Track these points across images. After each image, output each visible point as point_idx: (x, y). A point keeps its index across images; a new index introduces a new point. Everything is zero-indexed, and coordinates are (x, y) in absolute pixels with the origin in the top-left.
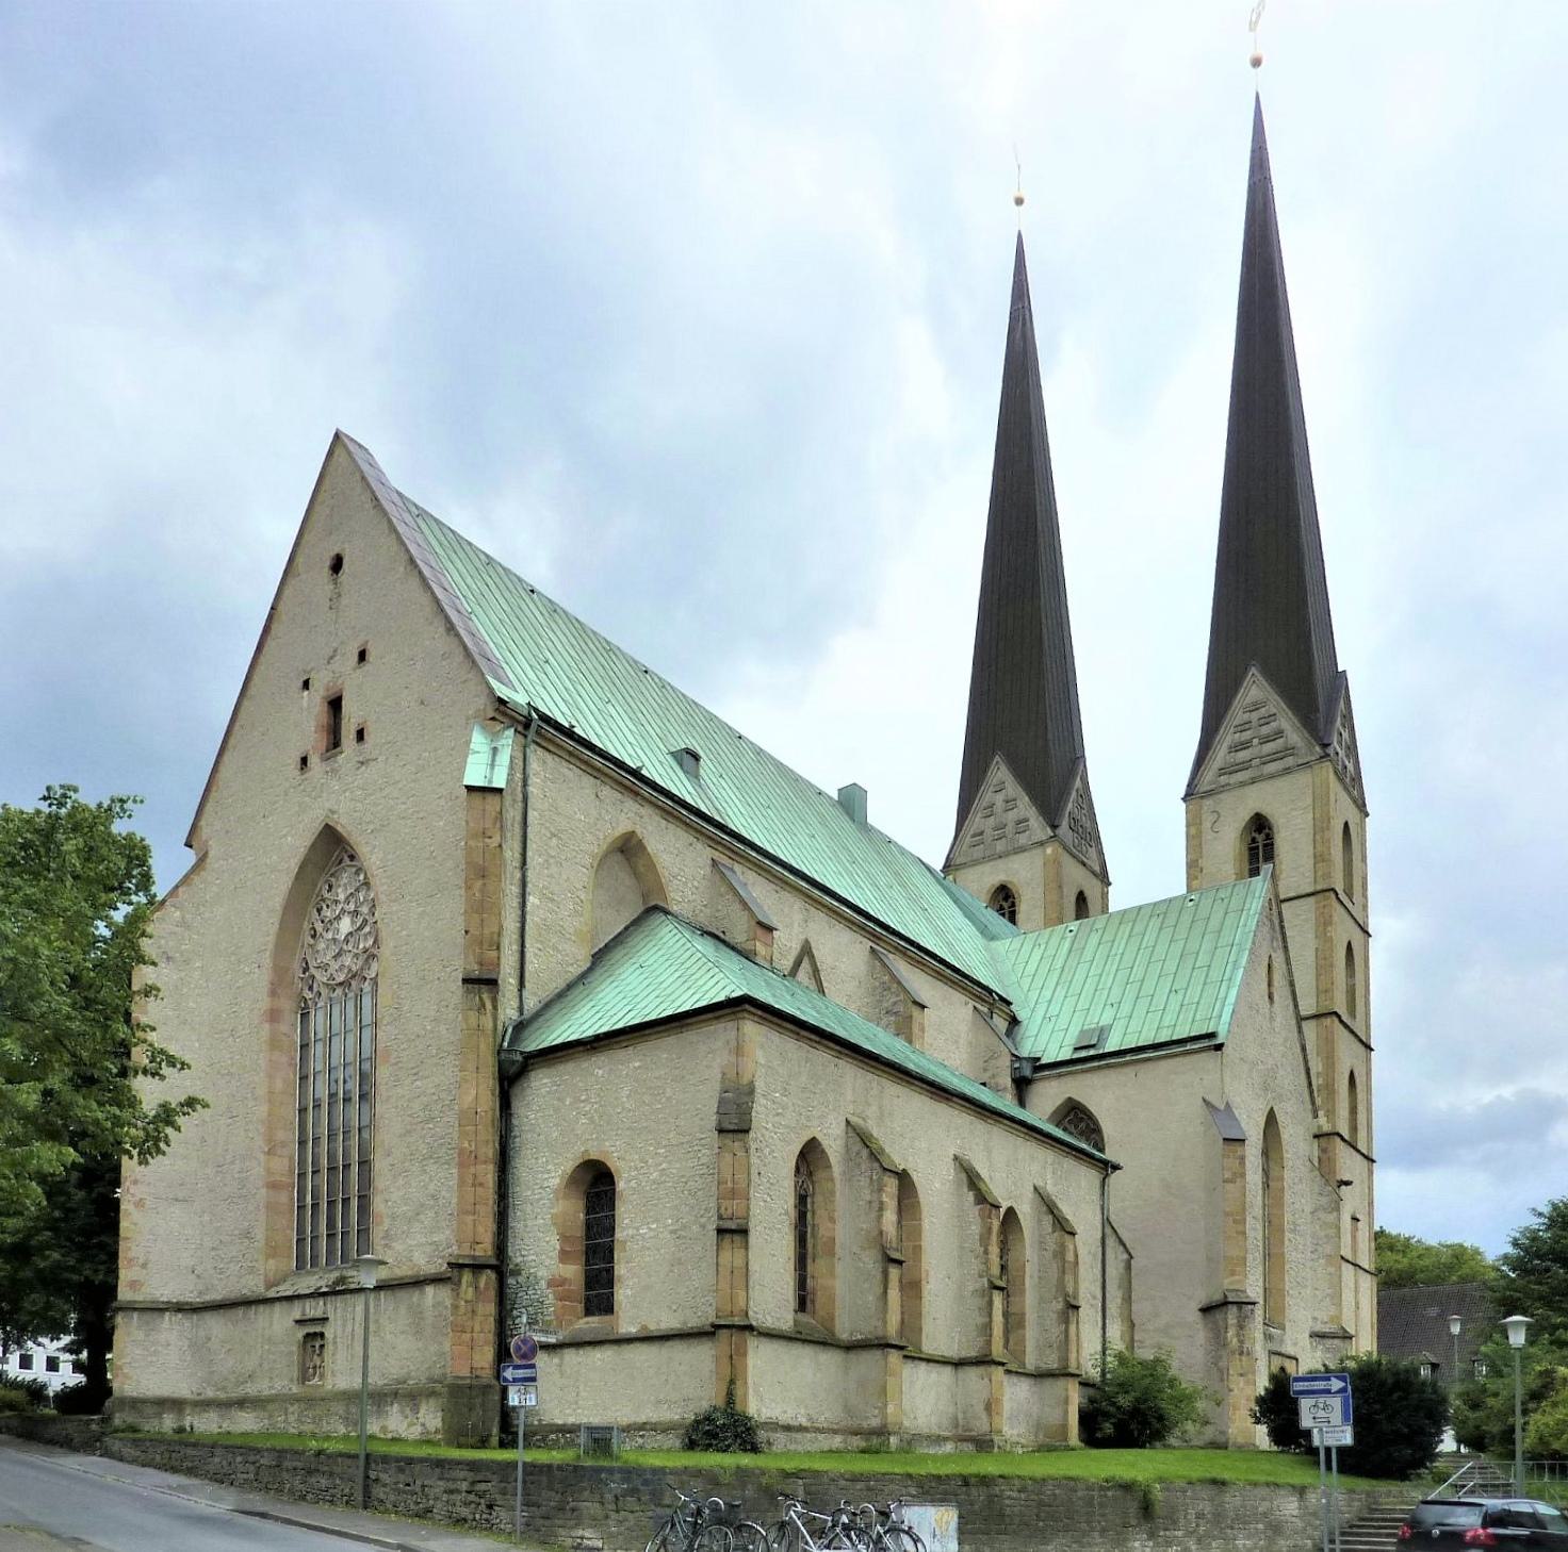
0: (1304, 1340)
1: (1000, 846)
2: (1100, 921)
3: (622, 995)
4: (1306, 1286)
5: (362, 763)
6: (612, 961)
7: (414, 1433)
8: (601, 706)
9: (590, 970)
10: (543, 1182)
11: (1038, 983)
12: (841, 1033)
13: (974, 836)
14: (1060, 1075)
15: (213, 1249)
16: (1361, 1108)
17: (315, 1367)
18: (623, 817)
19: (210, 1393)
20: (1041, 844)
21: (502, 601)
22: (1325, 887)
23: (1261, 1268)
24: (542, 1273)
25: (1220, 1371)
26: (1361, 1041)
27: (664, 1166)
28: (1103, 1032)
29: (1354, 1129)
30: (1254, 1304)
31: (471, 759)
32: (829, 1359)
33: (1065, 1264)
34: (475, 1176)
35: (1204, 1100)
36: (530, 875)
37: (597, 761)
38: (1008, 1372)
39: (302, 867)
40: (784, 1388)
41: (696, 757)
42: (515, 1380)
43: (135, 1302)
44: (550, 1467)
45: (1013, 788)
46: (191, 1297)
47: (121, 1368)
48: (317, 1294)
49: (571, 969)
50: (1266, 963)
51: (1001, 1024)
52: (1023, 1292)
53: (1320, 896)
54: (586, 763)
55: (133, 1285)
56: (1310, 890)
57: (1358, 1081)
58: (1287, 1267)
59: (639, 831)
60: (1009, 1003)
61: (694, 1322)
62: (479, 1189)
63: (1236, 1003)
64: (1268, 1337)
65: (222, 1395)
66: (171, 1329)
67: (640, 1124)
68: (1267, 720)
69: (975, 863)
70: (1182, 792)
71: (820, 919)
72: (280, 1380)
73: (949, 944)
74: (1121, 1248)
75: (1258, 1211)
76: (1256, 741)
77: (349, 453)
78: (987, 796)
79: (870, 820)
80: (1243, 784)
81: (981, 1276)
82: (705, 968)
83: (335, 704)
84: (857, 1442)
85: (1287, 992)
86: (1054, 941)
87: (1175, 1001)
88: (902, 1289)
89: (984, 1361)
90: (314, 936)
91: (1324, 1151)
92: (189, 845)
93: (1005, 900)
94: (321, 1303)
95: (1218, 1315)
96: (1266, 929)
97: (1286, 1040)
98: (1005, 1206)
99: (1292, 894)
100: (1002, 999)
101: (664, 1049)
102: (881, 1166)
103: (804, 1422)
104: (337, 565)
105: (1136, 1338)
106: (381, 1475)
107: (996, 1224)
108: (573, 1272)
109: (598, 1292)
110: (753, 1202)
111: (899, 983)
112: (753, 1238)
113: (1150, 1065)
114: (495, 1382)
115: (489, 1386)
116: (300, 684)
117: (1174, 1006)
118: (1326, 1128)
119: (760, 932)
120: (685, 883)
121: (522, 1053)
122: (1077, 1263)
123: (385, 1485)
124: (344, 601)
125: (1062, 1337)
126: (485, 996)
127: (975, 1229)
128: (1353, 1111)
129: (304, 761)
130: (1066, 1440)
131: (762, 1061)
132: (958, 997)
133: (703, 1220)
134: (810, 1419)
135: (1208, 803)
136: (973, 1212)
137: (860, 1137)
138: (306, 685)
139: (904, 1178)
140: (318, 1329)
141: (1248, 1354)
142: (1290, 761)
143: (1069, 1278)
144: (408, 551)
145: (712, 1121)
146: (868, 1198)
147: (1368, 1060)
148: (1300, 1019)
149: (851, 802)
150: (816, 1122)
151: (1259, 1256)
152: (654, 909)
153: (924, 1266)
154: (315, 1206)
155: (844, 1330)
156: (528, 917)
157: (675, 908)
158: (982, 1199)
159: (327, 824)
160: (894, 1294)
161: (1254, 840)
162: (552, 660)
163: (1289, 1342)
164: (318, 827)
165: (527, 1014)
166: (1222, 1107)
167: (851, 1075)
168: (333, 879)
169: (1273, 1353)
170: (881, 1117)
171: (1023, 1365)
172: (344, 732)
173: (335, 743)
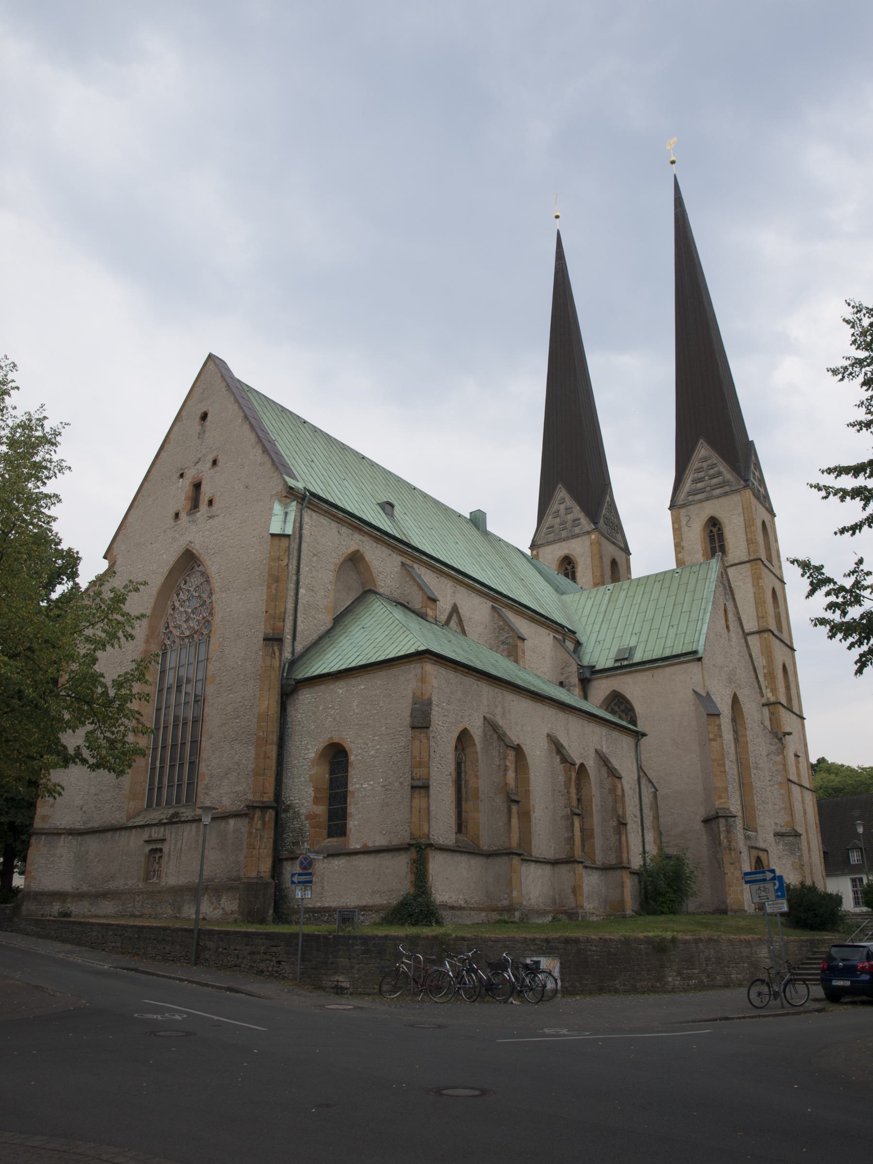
0: (770, 837)
1: (564, 534)
2: (626, 584)
3: (353, 645)
5: (210, 517)
7: (218, 913)
9: (333, 628)
10: (305, 753)
11: (591, 620)
14: (607, 677)
16: (793, 686)
17: (154, 871)
19: (85, 888)
20: (588, 533)
21: (289, 430)
24: (303, 811)
27: (378, 747)
28: (631, 650)
29: (789, 699)
30: (735, 817)
31: (273, 518)
32: (476, 862)
33: (616, 797)
34: (265, 752)
37: (340, 514)
38: (586, 867)
39: (171, 572)
40: (452, 882)
41: (392, 506)
42: (299, 882)
43: (44, 829)
45: (569, 502)
46: (79, 826)
48: (160, 824)
51: (570, 645)
52: (592, 816)
53: (753, 563)
54: (334, 516)
55: (44, 818)
56: (747, 559)
57: (788, 669)
60: (574, 633)
61: (395, 842)
63: (707, 633)
64: (748, 838)
65: (93, 890)
67: (369, 725)
69: (550, 543)
70: (668, 504)
71: (462, 590)
73: (537, 600)
74: (650, 785)
75: (733, 757)
76: (707, 478)
77: (216, 364)
78: (554, 506)
80: (701, 501)
81: (566, 807)
82: (401, 631)
83: (197, 486)
84: (495, 916)
85: (737, 624)
87: (672, 631)
88: (519, 818)
89: (570, 861)
90: (173, 609)
91: (772, 714)
92: (105, 557)
93: (568, 566)
94: (162, 830)
96: (721, 589)
97: (740, 652)
98: (578, 762)
99: (737, 561)
100: (570, 630)
101: (378, 680)
102: (505, 744)
103: (462, 902)
104: (204, 417)
105: (663, 840)
106: (208, 943)
107: (574, 775)
108: (321, 810)
109: (337, 821)
110: (431, 769)
111: (509, 626)
112: (432, 791)
113: (659, 670)
114: (270, 880)
116: (178, 475)
118: (772, 699)
119: (429, 603)
120: (386, 577)
121: (295, 679)
122: (623, 795)
124: (207, 434)
125: (617, 843)
126: (275, 648)
127: (561, 778)
128: (788, 687)
129: (177, 515)
130: (624, 911)
131: (436, 685)
133: (402, 780)
134: (466, 902)
135: (683, 511)
136: (560, 768)
137: (491, 726)
138: (182, 476)
139: (518, 750)
140: (159, 846)
141: (735, 850)
142: (727, 489)
143: (619, 805)
146: (498, 763)
147: (793, 658)
148: (746, 635)
149: (477, 520)
151: (736, 785)
152: (369, 592)
153: (532, 802)
154: (162, 768)
156: (300, 601)
157: (381, 591)
158: (565, 759)
160: (515, 821)
161: (711, 531)
163: (760, 840)
164: (181, 550)
165: (296, 655)
166: (704, 695)
167: (486, 690)
169: (752, 847)
170: (504, 714)
171: (594, 862)
172: (201, 501)
173: (195, 504)
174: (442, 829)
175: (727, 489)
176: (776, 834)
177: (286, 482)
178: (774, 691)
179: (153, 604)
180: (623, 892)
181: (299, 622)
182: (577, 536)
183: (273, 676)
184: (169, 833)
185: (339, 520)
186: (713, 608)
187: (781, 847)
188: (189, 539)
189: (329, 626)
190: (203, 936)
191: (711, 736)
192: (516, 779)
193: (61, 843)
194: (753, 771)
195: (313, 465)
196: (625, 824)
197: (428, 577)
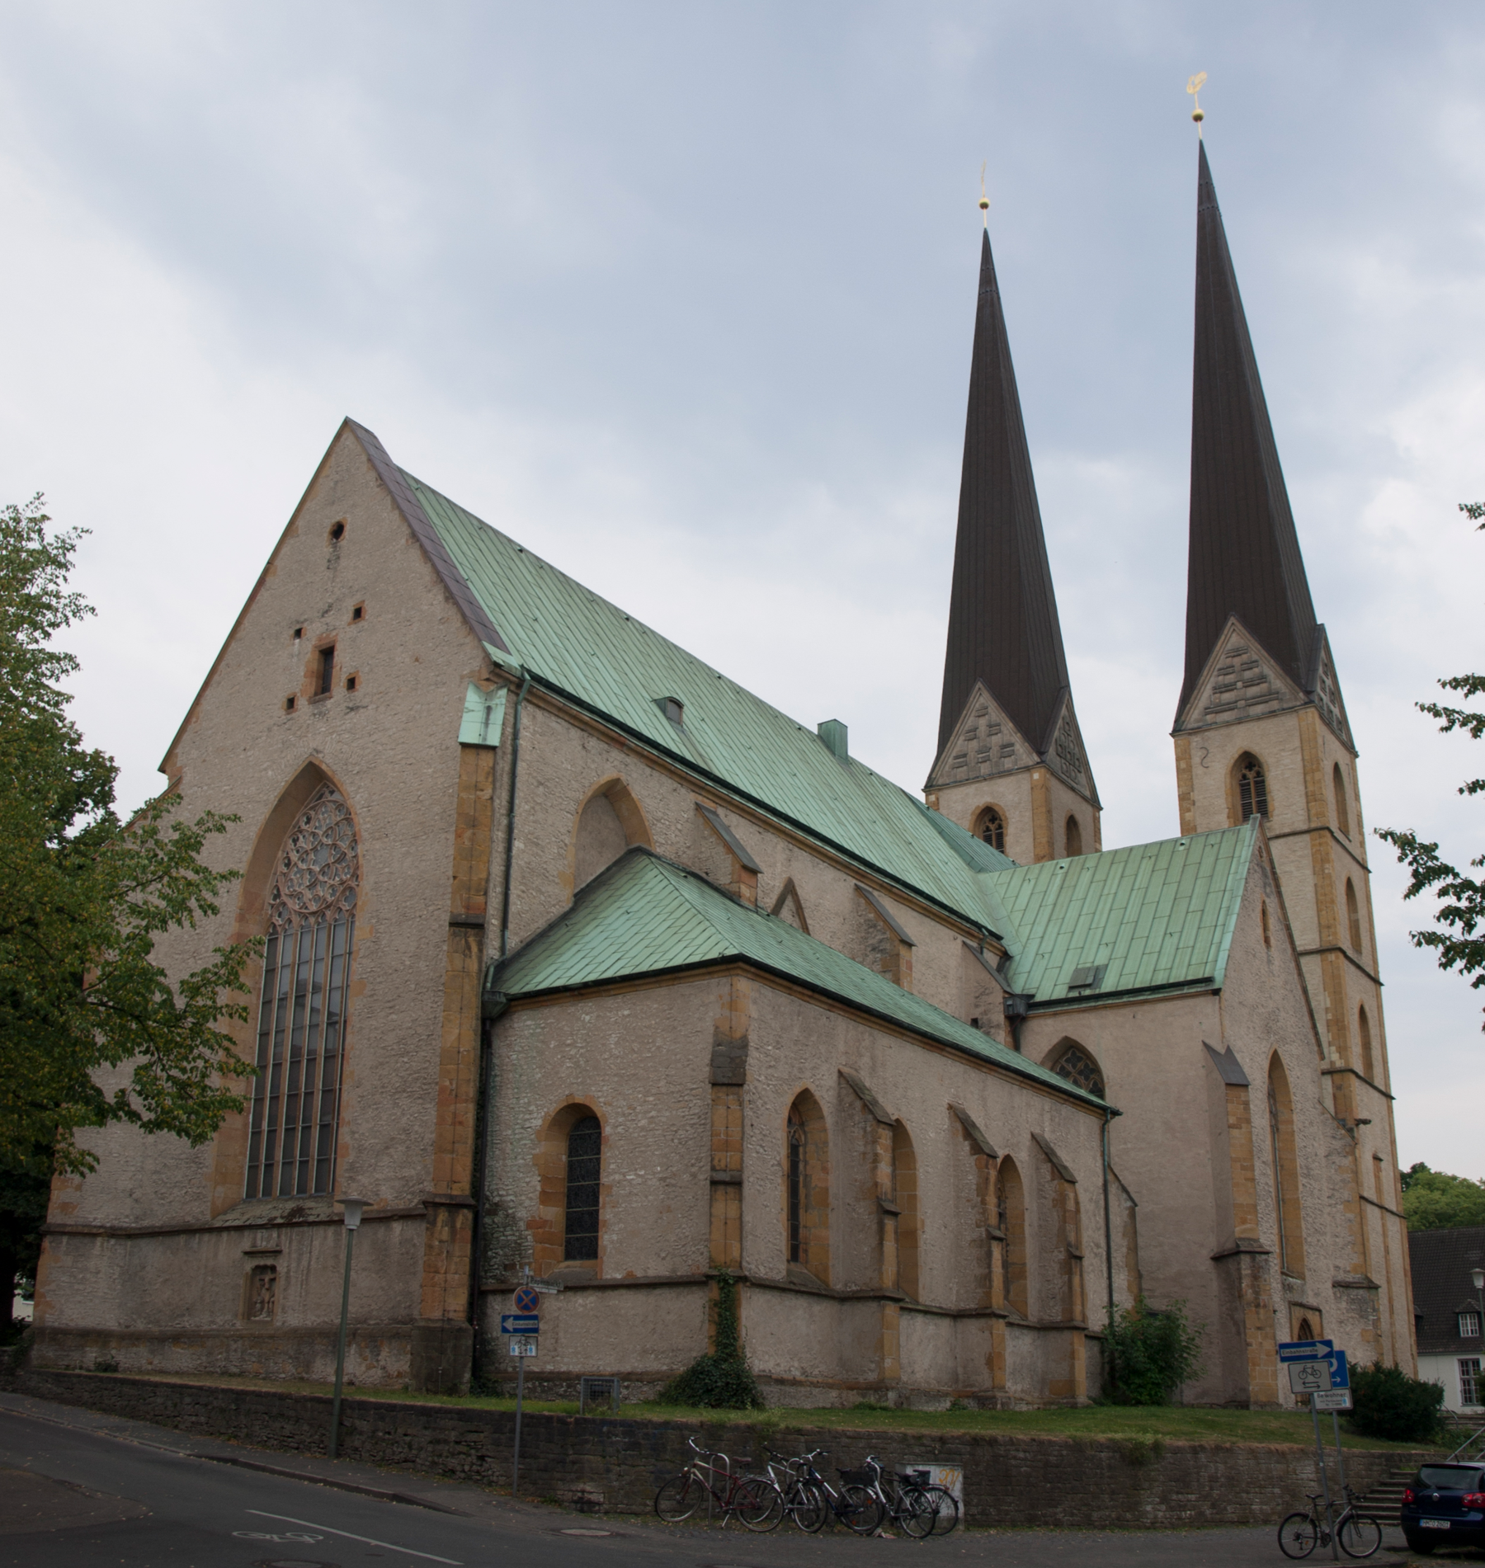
0: (1327, 1289)
1: (985, 769)
2: (1091, 860)
4: (1324, 1234)
5: (352, 709)
6: (596, 903)
7: (376, 1375)
8: (586, 658)
9: (573, 910)
11: (1029, 917)
12: (832, 986)
13: (956, 757)
14: (1055, 1014)
15: (156, 1172)
16: (1375, 1044)
18: (608, 766)
19: (140, 1326)
20: (1028, 769)
22: (1319, 825)
23: (1274, 1215)
24: (522, 1214)
25: (1236, 1323)
26: (1369, 976)
27: (653, 1113)
28: (1099, 972)
30: (1267, 1253)
31: (466, 717)
32: (823, 1311)
33: (1066, 1213)
35: (1205, 1044)
36: (517, 821)
38: (1010, 1324)
40: (781, 1340)
41: (679, 705)
43: (65, 1225)
44: (549, 1419)
45: (996, 714)
46: (127, 1222)
47: (43, 1296)
48: (271, 1225)
49: (553, 909)
50: (1259, 909)
51: (992, 959)
52: (1022, 1241)
53: (1315, 834)
54: (575, 717)
55: (65, 1207)
56: (1304, 827)
57: (1369, 1015)
58: (1303, 1213)
59: (623, 778)
60: (999, 938)
61: (683, 1271)
62: (459, 1128)
63: (1231, 949)
64: (1288, 1288)
65: (155, 1329)
66: (102, 1259)
67: (640, 1078)
68: (1250, 665)
69: (959, 783)
71: (803, 860)
72: (224, 1316)
73: (936, 880)
75: (1268, 1156)
76: (1239, 684)
78: (969, 720)
79: (850, 753)
80: (1228, 724)
81: (978, 1226)
83: (327, 653)
84: (854, 1398)
85: (1283, 935)
86: (1045, 876)
87: (1171, 943)
88: (897, 1241)
89: (983, 1313)
90: (288, 865)
91: (1338, 1088)
92: (162, 769)
94: (275, 1235)
95: (1231, 1264)
96: (1257, 876)
97: (1286, 983)
98: (1001, 1153)
100: (991, 933)
101: (654, 1001)
102: (875, 1118)
103: (797, 1374)
104: (338, 531)
106: (357, 1422)
107: (993, 1174)
108: (554, 1213)
109: (581, 1233)
111: (885, 921)
112: (748, 1190)
113: (1146, 1007)
114: (466, 1325)
115: (460, 1330)
116: (292, 632)
117: (1169, 948)
118: (1339, 1064)
119: (745, 876)
120: (668, 827)
122: (1078, 1211)
123: (361, 1433)
124: (343, 562)
125: (1066, 1289)
126: (471, 939)
127: (972, 1179)
128: (1367, 1046)
129: (291, 703)
130: (1073, 1397)
131: (755, 1015)
132: (945, 933)
133: (694, 1170)
134: (804, 1373)
135: (1196, 740)
136: (969, 1161)
137: (852, 1088)
138: (298, 633)
139: (898, 1129)
140: (269, 1262)
141: (1265, 1306)
142: (1275, 705)
143: (1070, 1227)
144: (410, 526)
145: (706, 1071)
146: (862, 1149)
147: (1378, 996)
148: (1298, 955)
149: (832, 737)
150: (808, 1074)
151: (1271, 1202)
152: (635, 853)
153: (920, 1215)
155: (838, 1280)
156: (514, 861)
157: (659, 850)
159: (311, 764)
160: (890, 1246)
161: (1244, 777)
162: (541, 618)
163: (1310, 1293)
164: (300, 764)
165: (508, 954)
166: (1223, 1051)
167: (843, 1028)
168: (312, 813)
170: (873, 1069)
171: (1025, 1317)
172: (334, 680)
173: (323, 686)
174: (765, 1251)
175: (1275, 705)
176: (1337, 1285)
177: (487, 655)
178: (1343, 1050)
179: (250, 854)
180: (1072, 1367)
181: (513, 898)
182: (1008, 773)
183: (467, 988)
184: (287, 1240)
185: (584, 726)
186: (1243, 907)
187: (1344, 1305)
188: (313, 745)
189: (567, 906)
190: (349, 1411)
191: (1232, 1120)
192: (894, 1176)
193: (97, 1250)
194: (1302, 1180)
195: (536, 626)
196: (1080, 1258)
197: (743, 831)
